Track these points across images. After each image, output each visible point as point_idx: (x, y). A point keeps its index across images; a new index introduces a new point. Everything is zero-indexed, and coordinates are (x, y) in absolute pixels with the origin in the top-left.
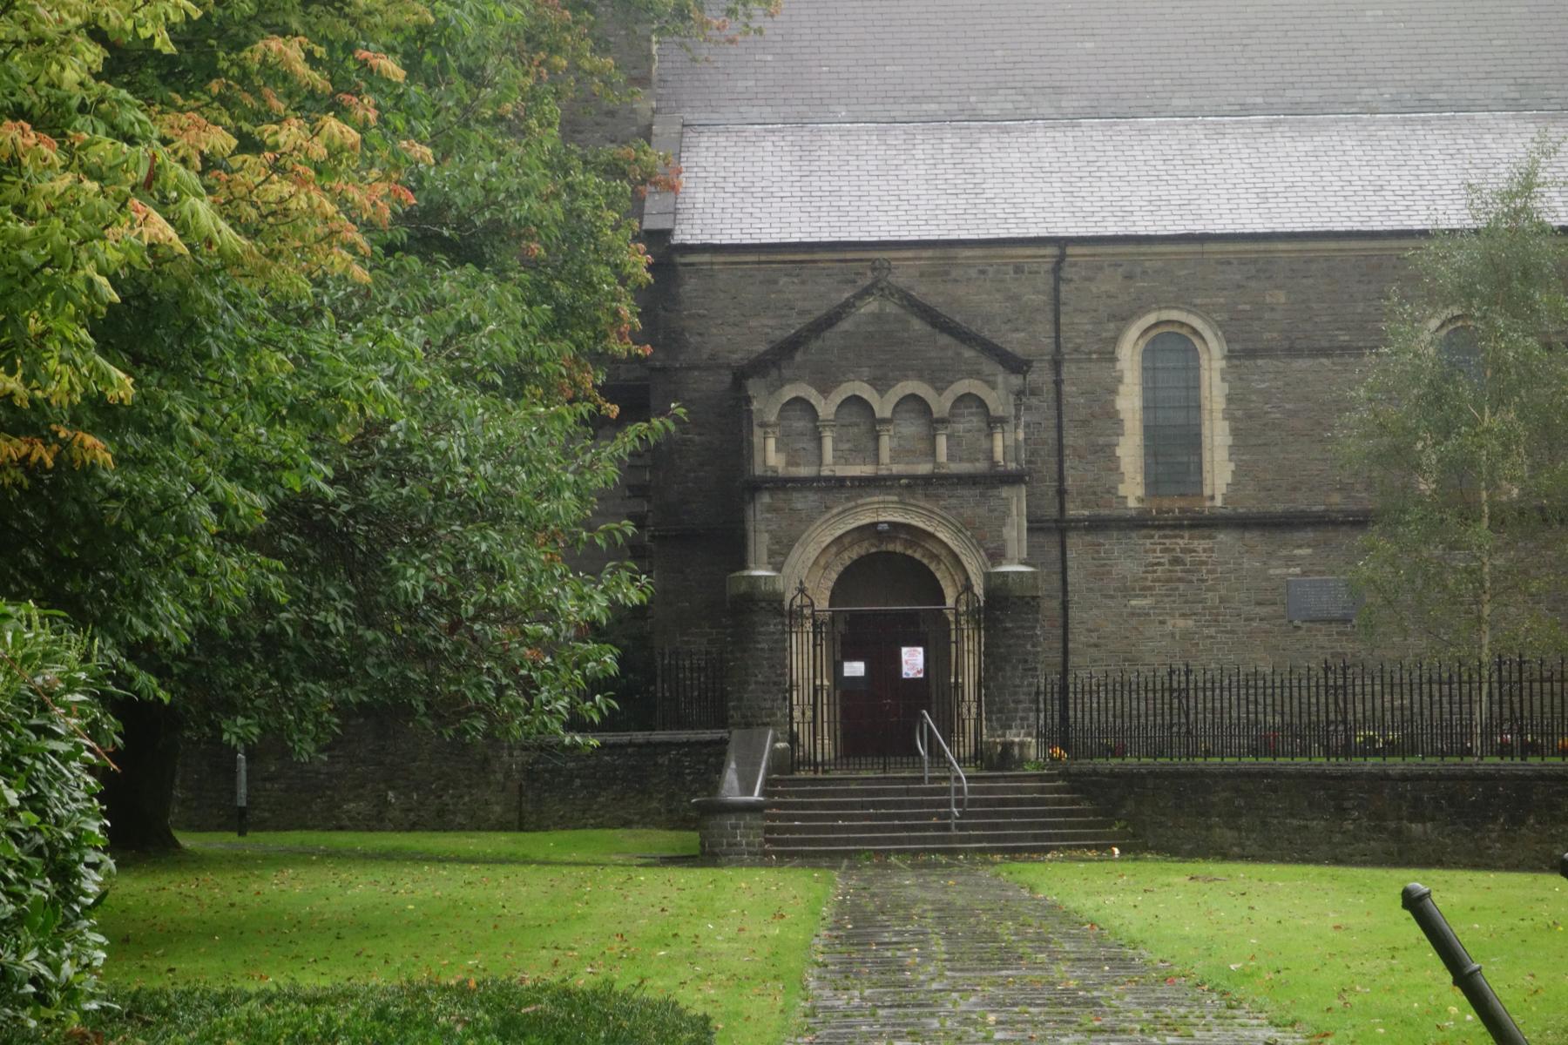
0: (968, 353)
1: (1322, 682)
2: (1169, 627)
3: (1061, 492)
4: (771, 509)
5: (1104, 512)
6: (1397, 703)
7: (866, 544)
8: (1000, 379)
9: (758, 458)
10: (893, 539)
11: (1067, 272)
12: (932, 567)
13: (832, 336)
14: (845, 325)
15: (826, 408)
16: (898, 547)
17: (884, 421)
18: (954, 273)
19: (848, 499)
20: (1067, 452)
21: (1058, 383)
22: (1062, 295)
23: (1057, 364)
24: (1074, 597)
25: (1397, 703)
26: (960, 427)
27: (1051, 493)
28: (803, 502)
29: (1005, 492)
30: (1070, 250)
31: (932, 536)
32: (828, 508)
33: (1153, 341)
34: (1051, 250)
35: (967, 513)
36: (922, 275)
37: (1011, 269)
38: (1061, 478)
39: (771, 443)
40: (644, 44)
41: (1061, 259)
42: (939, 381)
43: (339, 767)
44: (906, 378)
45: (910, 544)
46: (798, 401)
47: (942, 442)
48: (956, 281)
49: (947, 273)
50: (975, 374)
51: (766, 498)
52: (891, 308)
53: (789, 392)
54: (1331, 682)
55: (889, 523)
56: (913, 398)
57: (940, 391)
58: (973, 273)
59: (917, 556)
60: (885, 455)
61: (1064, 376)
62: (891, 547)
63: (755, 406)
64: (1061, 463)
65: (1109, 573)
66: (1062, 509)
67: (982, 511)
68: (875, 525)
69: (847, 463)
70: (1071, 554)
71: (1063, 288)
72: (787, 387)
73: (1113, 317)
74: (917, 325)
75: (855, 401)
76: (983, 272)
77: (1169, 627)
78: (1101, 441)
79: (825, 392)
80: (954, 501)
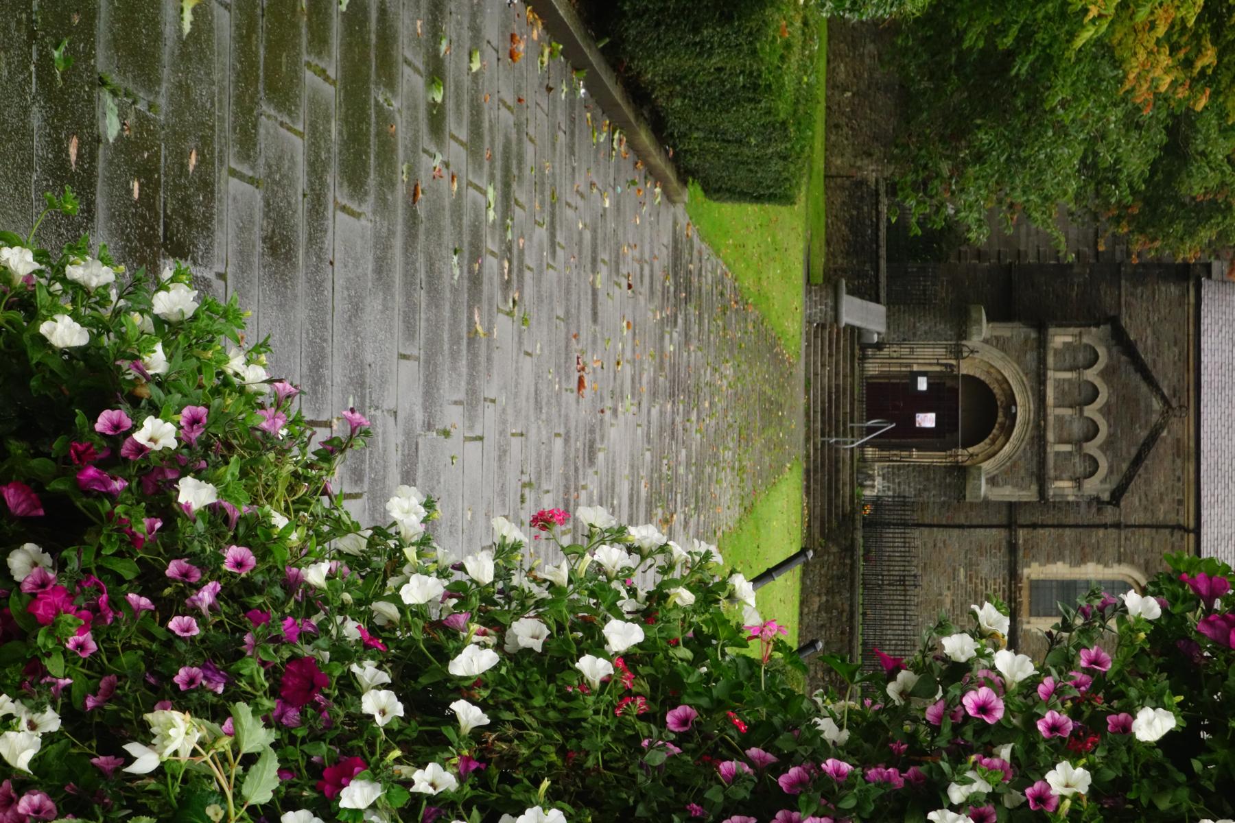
0: (1124, 466)
2: (946, 592)
3: (1034, 526)
4: (1027, 339)
5: (1021, 553)
7: (1003, 398)
8: (1107, 486)
9: (1059, 330)
10: (1005, 416)
11: (1178, 534)
12: (987, 441)
13: (1136, 378)
14: (1144, 388)
15: (1091, 375)
16: (1000, 419)
17: (1081, 411)
18: (1179, 462)
19: (1032, 387)
20: (1060, 530)
21: (1105, 526)
22: (1163, 531)
23: (1117, 526)
24: (966, 532)
26: (1077, 460)
27: (1034, 519)
28: (1031, 357)
29: (1034, 488)
30: (1192, 536)
31: (1007, 440)
32: (1026, 375)
34: (1192, 524)
35: (1021, 463)
36: (1178, 440)
37: (1180, 497)
38: (1043, 526)
39: (1069, 339)
42: (1107, 446)
44: (1110, 426)
45: (1002, 426)
46: (1097, 357)
47: (1067, 448)
48: (1174, 461)
49: (1179, 456)
50: (1111, 471)
51: (1033, 335)
52: (1155, 418)
53: (1102, 351)
55: (1015, 414)
56: (1097, 430)
57: (1101, 447)
58: (1178, 473)
59: (994, 431)
61: (1110, 530)
62: (1000, 414)
63: (1094, 330)
64: (1053, 526)
65: (981, 555)
67: (1022, 472)
68: (1015, 404)
71: (1167, 531)
72: (1104, 350)
73: (1147, 562)
74: (1143, 434)
75: (1095, 393)
76: (1179, 479)
77: (946, 592)
78: (1067, 552)
80: (1029, 455)
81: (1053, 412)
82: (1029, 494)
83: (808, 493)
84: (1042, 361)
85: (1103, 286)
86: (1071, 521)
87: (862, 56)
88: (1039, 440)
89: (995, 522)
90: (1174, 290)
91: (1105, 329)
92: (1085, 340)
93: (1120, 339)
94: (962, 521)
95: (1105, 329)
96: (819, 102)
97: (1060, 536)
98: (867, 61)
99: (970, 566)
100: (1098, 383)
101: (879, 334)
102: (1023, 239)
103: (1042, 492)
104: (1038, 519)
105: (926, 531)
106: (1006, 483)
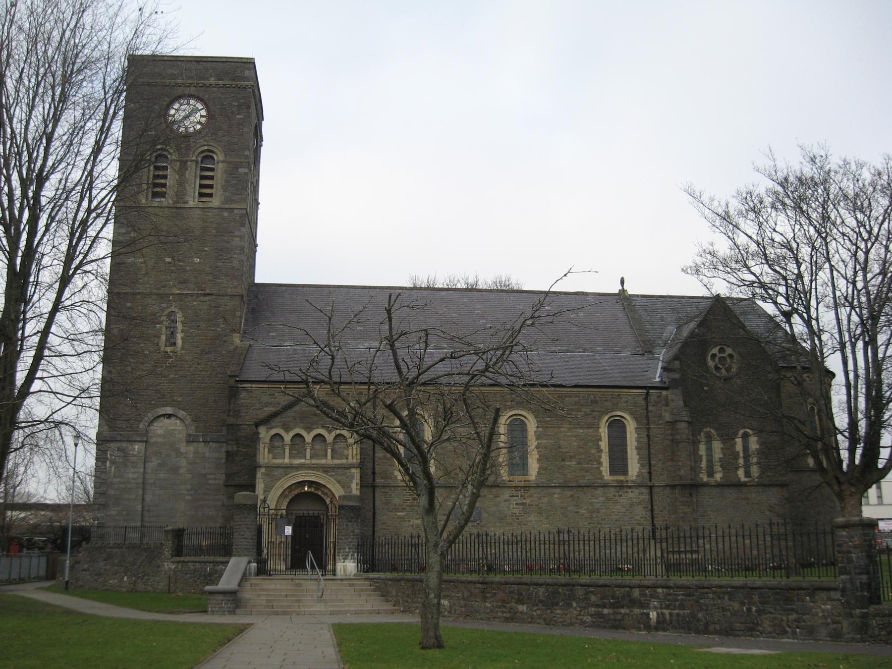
1: (557, 539)
2: (411, 523)
3: (374, 473)
6: (493, 551)
15: (288, 437)
24: (377, 511)
25: (493, 551)
27: (370, 473)
31: (324, 486)
33: (511, 422)
38: (374, 468)
40: (780, 334)
41: (647, 393)
43: (108, 567)
45: (316, 489)
46: (277, 435)
53: (274, 431)
54: (561, 538)
56: (319, 435)
59: (320, 493)
60: (308, 456)
66: (374, 480)
69: (295, 458)
70: (377, 496)
75: (298, 435)
77: (411, 523)
79: (287, 431)
81: (307, 461)
82: (356, 472)
83: (428, 289)
84: (278, 467)
85: (239, 434)
86: (371, 453)
87: (106, 570)
88: (326, 469)
89: (371, 495)
90: (243, 395)
91: (262, 430)
92: (267, 440)
93: (267, 421)
94: (371, 514)
95: (262, 430)
96: (833, 375)
97: (380, 459)
98: (108, 567)
99: (397, 510)
100: (292, 434)
101: (249, 562)
102: (217, 482)
103: (352, 466)
104: (370, 472)
105: (376, 534)
106: (350, 487)
